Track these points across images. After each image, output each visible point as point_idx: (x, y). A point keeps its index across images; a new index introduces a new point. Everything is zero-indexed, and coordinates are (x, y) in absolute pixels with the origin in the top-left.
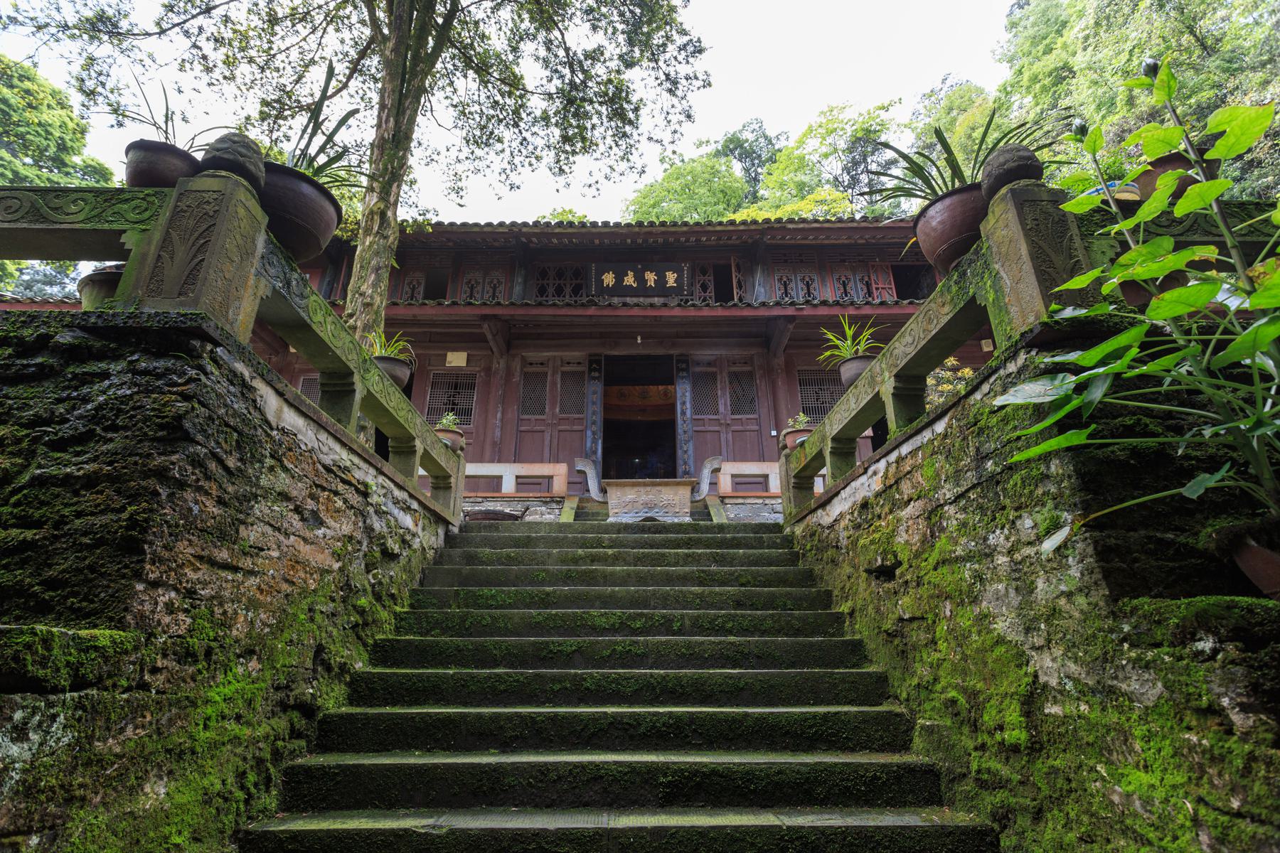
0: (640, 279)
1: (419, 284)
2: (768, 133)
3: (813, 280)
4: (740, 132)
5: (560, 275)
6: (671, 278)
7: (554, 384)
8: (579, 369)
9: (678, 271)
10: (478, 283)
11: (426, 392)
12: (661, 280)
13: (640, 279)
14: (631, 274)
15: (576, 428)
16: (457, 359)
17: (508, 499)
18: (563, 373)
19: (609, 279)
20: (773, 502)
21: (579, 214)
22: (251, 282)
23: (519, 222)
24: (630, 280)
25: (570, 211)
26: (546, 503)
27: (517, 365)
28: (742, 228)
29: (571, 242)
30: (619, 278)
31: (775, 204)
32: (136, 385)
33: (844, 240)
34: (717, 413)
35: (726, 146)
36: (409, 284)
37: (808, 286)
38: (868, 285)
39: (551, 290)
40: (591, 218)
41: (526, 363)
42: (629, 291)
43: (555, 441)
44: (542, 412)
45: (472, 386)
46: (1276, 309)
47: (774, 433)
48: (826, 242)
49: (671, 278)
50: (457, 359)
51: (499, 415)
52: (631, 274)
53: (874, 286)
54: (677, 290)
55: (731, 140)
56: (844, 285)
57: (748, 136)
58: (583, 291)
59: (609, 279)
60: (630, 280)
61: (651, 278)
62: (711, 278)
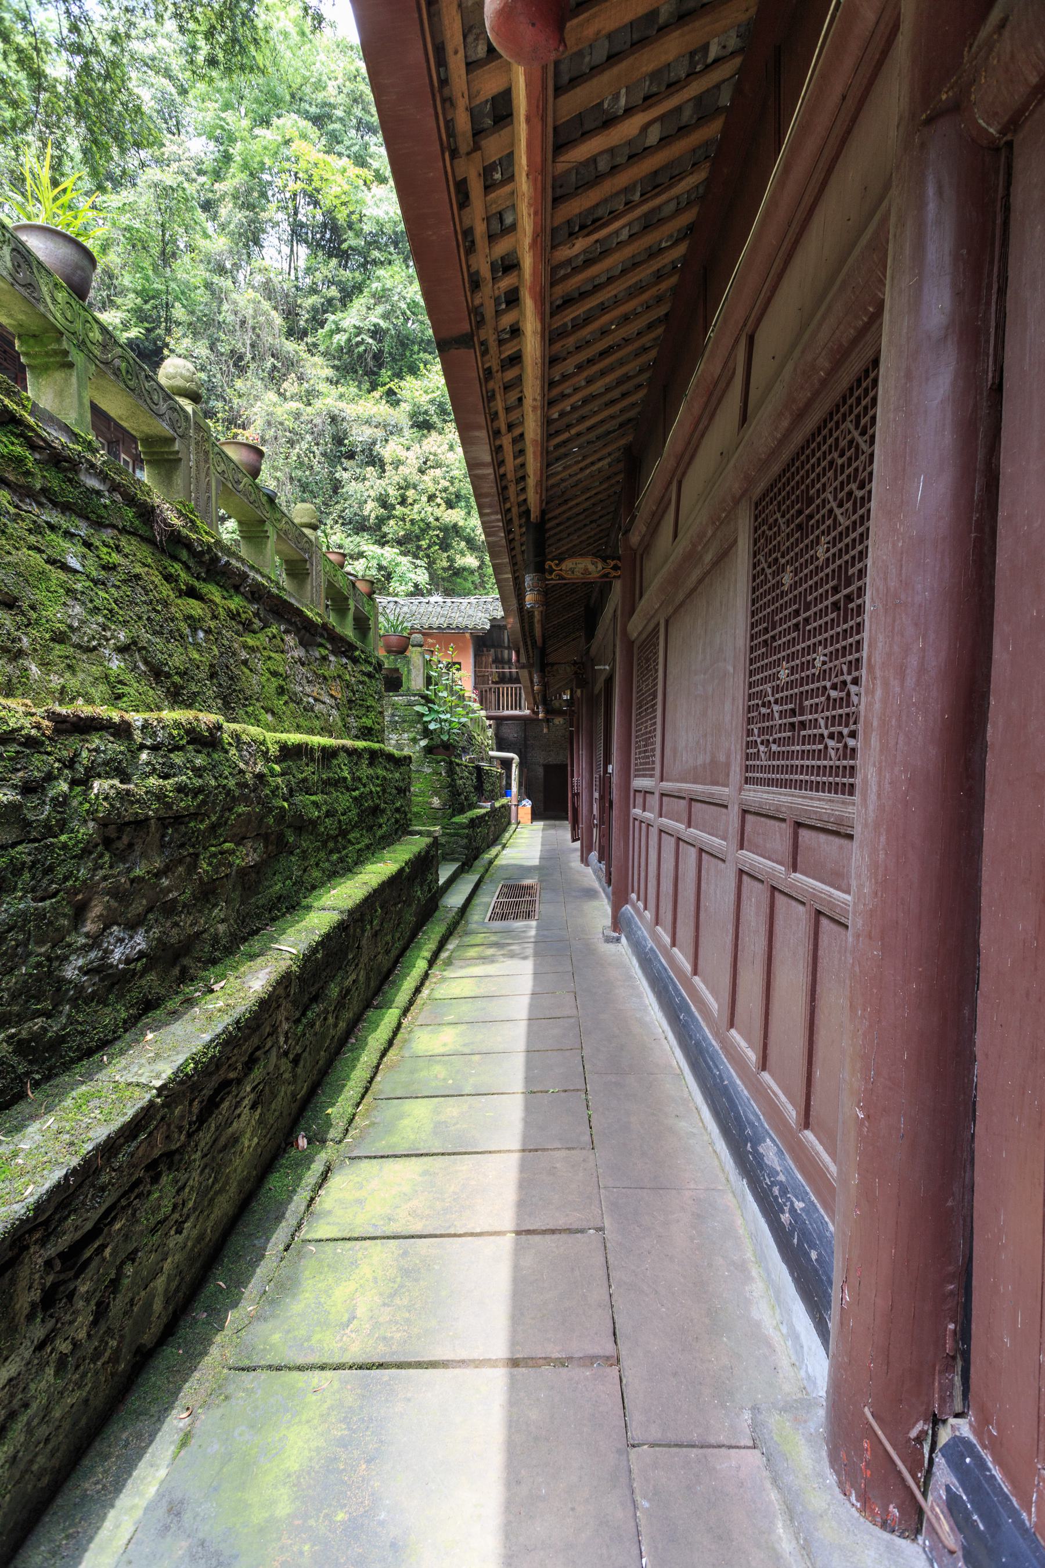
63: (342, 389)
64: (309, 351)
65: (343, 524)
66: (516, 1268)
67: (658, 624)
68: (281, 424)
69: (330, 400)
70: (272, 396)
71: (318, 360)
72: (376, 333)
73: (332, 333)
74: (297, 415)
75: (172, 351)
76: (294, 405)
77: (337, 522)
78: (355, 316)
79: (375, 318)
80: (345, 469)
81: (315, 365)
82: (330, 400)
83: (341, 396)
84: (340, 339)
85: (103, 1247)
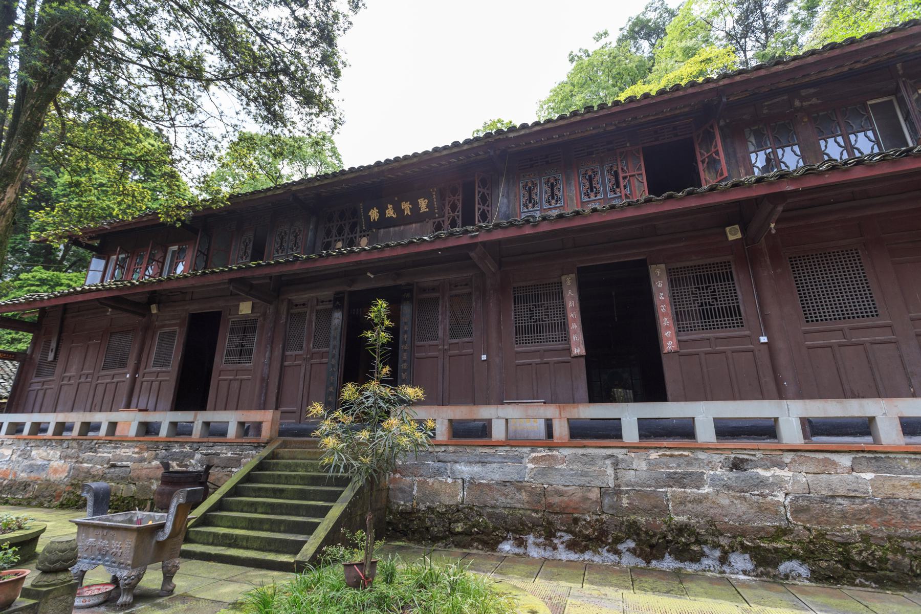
0: (398, 210)
2: (669, 7)
3: (557, 181)
4: (644, 14)
6: (423, 204)
10: (300, 231)
12: (415, 207)
13: (398, 210)
15: (324, 360)
16: (245, 308)
17: (230, 444)
18: (317, 311)
20: (437, 449)
21: (506, 121)
23: (441, 146)
24: (390, 213)
25: (499, 121)
27: (284, 308)
28: (465, 147)
29: (459, 160)
30: (382, 213)
31: (674, 71)
33: (590, 131)
34: (437, 338)
35: (632, 30)
37: (552, 187)
38: (616, 175)
39: (334, 231)
40: (420, 151)
41: (291, 305)
42: (391, 223)
43: (308, 374)
44: (301, 348)
45: (254, 330)
46: (6, 502)
48: (573, 137)
49: (423, 204)
50: (245, 308)
51: (268, 354)
52: (390, 206)
53: (621, 175)
54: (429, 215)
55: (635, 24)
56: (590, 180)
57: (652, 16)
58: (358, 229)
59: (374, 214)
61: (406, 207)
62: (460, 197)
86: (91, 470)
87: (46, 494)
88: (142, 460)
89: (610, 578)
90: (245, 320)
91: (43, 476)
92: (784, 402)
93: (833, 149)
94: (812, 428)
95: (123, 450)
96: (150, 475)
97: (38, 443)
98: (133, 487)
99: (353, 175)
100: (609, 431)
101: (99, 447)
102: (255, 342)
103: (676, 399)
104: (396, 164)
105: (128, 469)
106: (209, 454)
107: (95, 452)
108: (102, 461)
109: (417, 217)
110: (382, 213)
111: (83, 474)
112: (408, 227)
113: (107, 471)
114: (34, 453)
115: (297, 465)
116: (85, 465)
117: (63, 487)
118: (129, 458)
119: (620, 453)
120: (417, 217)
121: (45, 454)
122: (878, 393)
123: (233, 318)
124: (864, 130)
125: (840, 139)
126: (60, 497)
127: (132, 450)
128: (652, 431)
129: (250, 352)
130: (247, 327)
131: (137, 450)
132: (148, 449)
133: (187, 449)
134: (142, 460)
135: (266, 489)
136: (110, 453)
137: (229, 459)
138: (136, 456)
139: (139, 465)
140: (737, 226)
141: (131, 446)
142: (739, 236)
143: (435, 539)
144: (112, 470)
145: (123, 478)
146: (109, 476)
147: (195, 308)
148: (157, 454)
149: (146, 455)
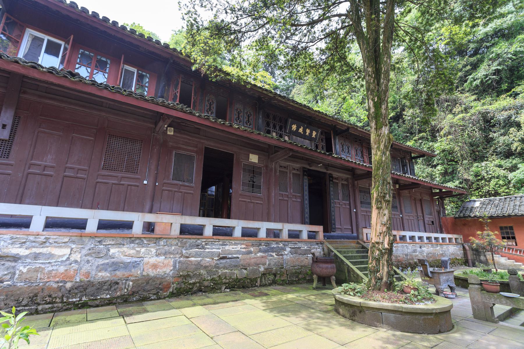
1: (213, 103)
5: (274, 118)
6: (314, 134)
7: (290, 178)
8: (298, 173)
9: (317, 132)
11: (241, 173)
12: (311, 134)
14: (302, 128)
16: (254, 158)
19: (294, 127)
22: (207, 250)
24: (301, 130)
26: (317, 244)
30: (298, 129)
32: (419, 3)
36: (208, 101)
47: (355, 210)
49: (314, 134)
52: (302, 128)
54: (314, 139)
59: (294, 127)
60: (301, 130)
61: (308, 131)
63: (482, 101)
64: (461, 93)
65: (496, 155)
66: (225, 218)
67: (289, 157)
68: (457, 125)
69: (478, 107)
70: (450, 116)
71: (467, 94)
72: (497, 72)
73: (471, 82)
74: (463, 119)
75: (406, 115)
76: (461, 116)
77: (493, 155)
78: (481, 72)
79: (495, 66)
80: (495, 132)
81: (466, 97)
82: (478, 107)
83: (484, 104)
84: (478, 82)
85: (199, 239)
86: (202, 263)
87: (148, 287)
88: (250, 252)
89: (149, 308)
90: (253, 165)
91: (137, 272)
92: (184, 217)
93: (83, 72)
94: (103, 225)
95: (231, 247)
96: (258, 262)
97: (120, 241)
98: (245, 271)
99: (308, 110)
100: (23, 223)
101: (206, 244)
102: (261, 181)
103: (235, 218)
104: (325, 116)
105: (238, 260)
106: (296, 248)
107: (203, 248)
108: (212, 255)
109: (310, 138)
110: (298, 129)
111: (194, 267)
112: (305, 140)
113: (218, 262)
114: (113, 251)
115: (348, 252)
116: (193, 259)
117: (172, 280)
118: (238, 252)
119: (407, 244)
120: (310, 138)
121: (132, 252)
122: (262, 220)
123: (244, 162)
124: (87, 66)
125: (89, 70)
126: (170, 287)
127: (239, 246)
128: (218, 232)
129: (259, 187)
130: (253, 170)
131: (243, 246)
132: (253, 245)
133: (281, 245)
134: (250, 252)
135: (358, 262)
136: (219, 249)
137: (306, 250)
138: (244, 250)
139: (248, 256)
140: (173, 129)
141: (238, 244)
142: (172, 133)
143: (195, 293)
144: (222, 261)
145: (236, 266)
146: (221, 265)
147: (212, 145)
148: (260, 249)
149: (252, 249)
